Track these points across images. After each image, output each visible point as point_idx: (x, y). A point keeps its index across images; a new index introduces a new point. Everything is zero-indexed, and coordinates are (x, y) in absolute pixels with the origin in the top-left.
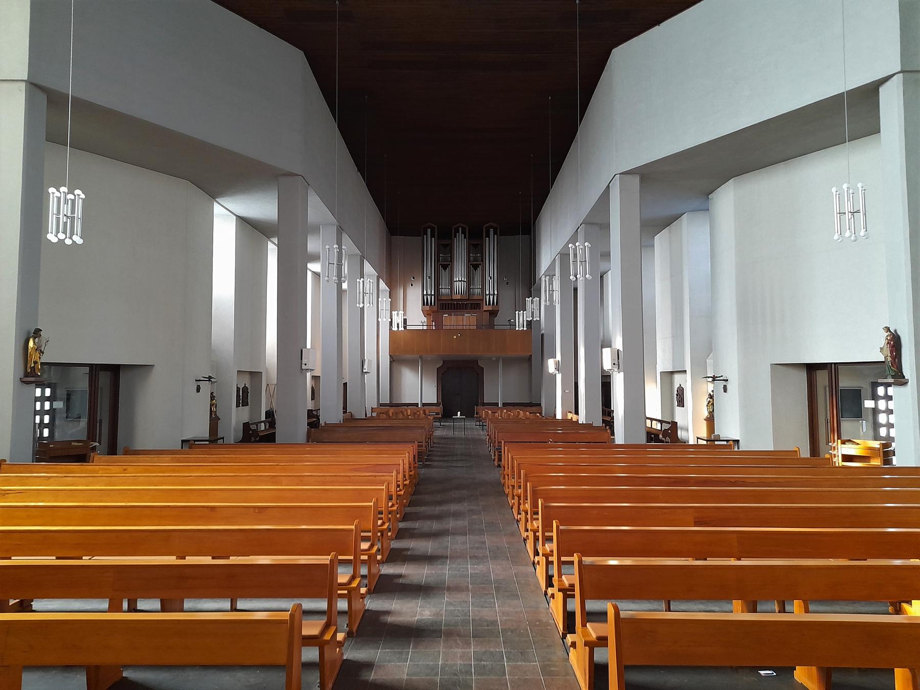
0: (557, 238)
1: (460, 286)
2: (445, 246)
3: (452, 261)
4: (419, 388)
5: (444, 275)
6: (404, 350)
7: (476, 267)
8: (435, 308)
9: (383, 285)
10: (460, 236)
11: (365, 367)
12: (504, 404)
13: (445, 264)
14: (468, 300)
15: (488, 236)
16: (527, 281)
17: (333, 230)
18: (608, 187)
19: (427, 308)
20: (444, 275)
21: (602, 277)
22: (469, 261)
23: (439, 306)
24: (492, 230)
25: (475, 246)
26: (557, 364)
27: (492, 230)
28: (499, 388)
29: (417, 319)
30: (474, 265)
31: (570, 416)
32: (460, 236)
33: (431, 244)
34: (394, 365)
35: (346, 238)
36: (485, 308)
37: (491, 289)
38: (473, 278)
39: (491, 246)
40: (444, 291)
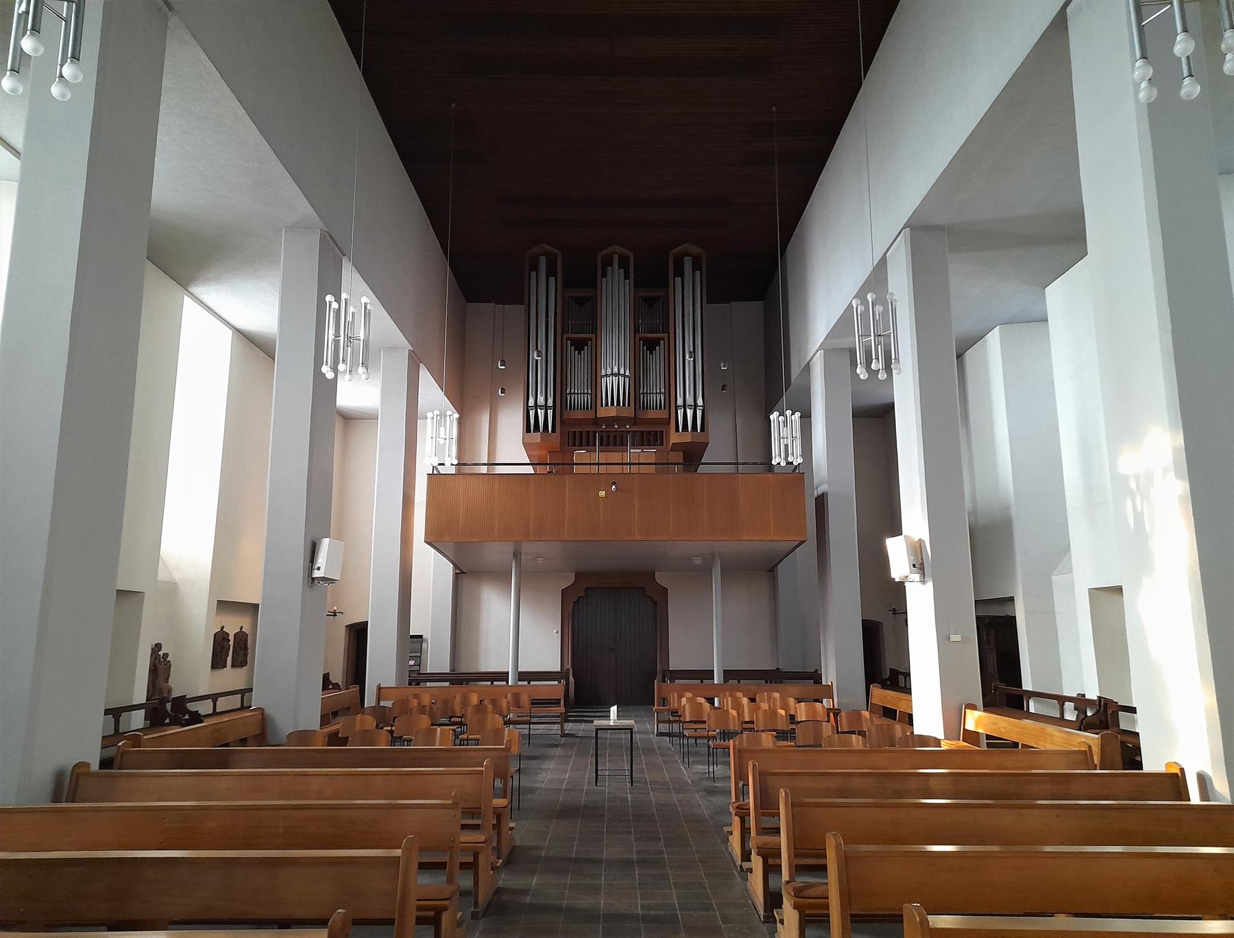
0: (851, 262)
1: (614, 378)
2: (581, 302)
3: (594, 329)
4: (522, 636)
5: (579, 363)
6: (470, 528)
7: (651, 345)
8: (556, 439)
9: (431, 392)
10: (616, 272)
11: (321, 561)
12: (728, 675)
13: (578, 334)
14: (635, 421)
15: (679, 272)
16: (768, 377)
17: (308, 250)
18: (883, 260)
19: (536, 437)
20: (579, 363)
21: (960, 356)
22: (636, 331)
23: (570, 433)
24: (688, 262)
25: (650, 302)
26: (916, 549)
27: (688, 262)
28: (706, 634)
29: (509, 445)
30: (650, 338)
31: (975, 720)
32: (616, 272)
33: (545, 294)
34: (466, 583)
35: (351, 278)
36: (674, 438)
37: (689, 395)
38: (646, 372)
39: (687, 297)
40: (579, 394)
